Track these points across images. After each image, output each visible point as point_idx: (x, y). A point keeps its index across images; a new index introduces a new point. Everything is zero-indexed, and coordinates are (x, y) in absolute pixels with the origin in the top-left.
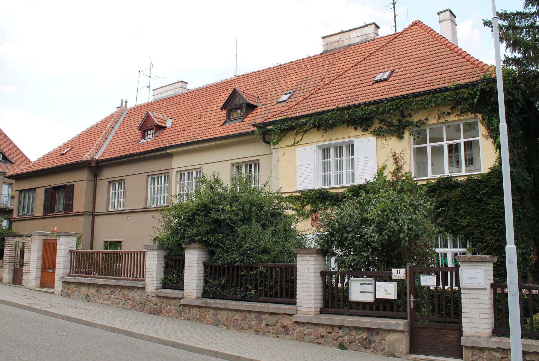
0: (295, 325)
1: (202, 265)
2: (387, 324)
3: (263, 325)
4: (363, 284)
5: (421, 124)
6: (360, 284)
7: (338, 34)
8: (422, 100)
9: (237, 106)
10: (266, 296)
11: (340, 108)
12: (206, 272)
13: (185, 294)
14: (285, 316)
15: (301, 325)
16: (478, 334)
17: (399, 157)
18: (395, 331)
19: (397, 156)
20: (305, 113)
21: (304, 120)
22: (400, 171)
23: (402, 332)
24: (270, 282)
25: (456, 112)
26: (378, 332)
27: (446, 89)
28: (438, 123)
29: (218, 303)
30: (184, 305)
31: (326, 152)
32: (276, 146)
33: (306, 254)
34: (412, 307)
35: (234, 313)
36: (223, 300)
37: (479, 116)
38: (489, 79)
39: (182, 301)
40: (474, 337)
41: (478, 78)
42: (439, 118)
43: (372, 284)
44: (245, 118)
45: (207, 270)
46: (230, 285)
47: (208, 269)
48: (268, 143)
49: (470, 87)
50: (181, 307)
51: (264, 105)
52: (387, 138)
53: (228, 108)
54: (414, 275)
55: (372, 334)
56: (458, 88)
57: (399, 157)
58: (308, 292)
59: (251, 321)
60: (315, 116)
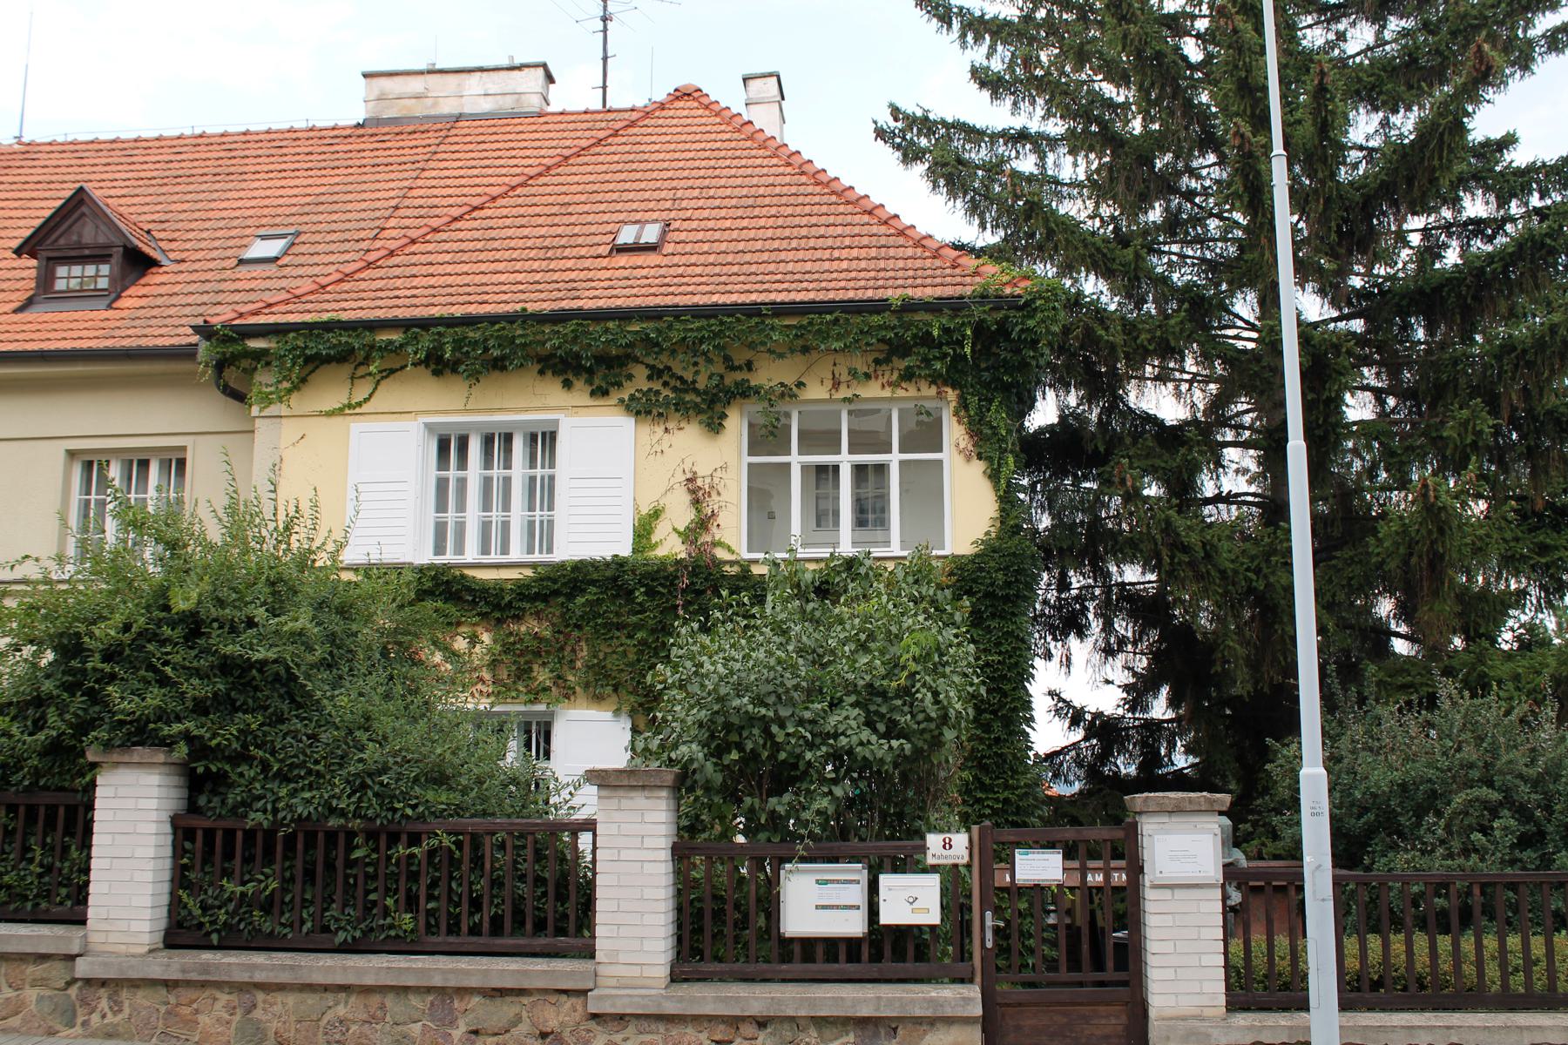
0: (592, 1025)
1: (168, 828)
2: (931, 1000)
3: (458, 1033)
4: (827, 882)
5: (782, 395)
6: (817, 882)
7: (421, 73)
8: (802, 327)
9: (87, 252)
10: (453, 929)
11: (532, 315)
12: (185, 851)
13: (95, 938)
14: (553, 999)
15: (612, 1025)
16: (1197, 1011)
17: (707, 487)
18: (950, 1021)
19: (699, 482)
20: (401, 313)
21: (396, 336)
22: (707, 529)
23: (967, 1021)
24: (471, 883)
25: (887, 374)
26: (895, 1030)
27: (879, 306)
28: (830, 400)
29: (233, 963)
30: (88, 982)
31: (449, 447)
32: (274, 409)
33: (633, 787)
34: (989, 945)
35: (330, 998)
36: (274, 954)
37: (952, 394)
38: (996, 297)
39: (82, 968)
40: (1184, 1018)
41: (968, 291)
42: (836, 385)
43: (858, 882)
44: (119, 297)
45: (188, 845)
46: (298, 900)
47: (193, 841)
48: (239, 397)
49: (946, 310)
50: (73, 991)
51: (183, 261)
52: (670, 425)
53: (45, 254)
54: (995, 854)
55: (876, 1035)
56: (909, 306)
57: (707, 487)
58: (642, 914)
59: (405, 1023)
60: (441, 329)
